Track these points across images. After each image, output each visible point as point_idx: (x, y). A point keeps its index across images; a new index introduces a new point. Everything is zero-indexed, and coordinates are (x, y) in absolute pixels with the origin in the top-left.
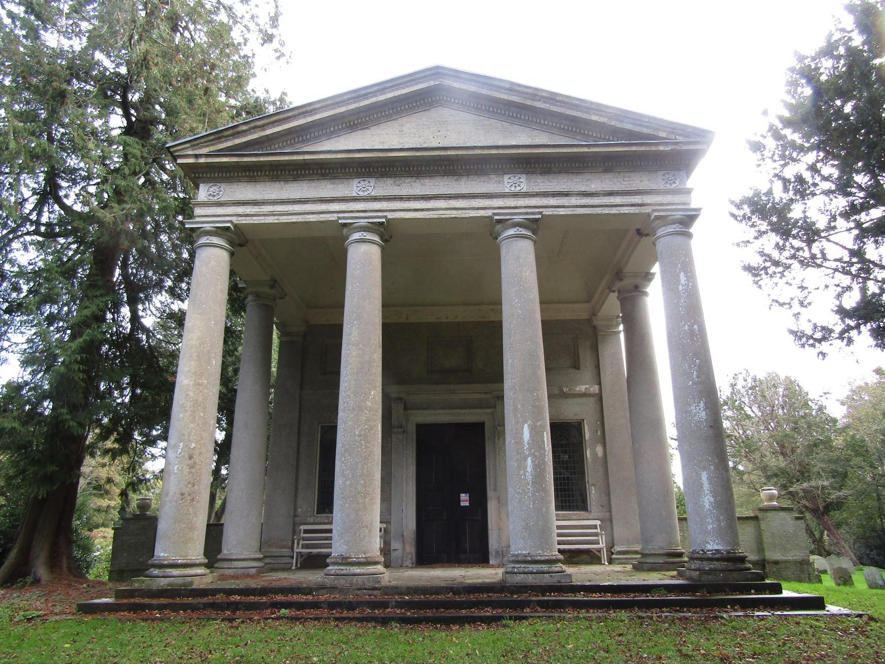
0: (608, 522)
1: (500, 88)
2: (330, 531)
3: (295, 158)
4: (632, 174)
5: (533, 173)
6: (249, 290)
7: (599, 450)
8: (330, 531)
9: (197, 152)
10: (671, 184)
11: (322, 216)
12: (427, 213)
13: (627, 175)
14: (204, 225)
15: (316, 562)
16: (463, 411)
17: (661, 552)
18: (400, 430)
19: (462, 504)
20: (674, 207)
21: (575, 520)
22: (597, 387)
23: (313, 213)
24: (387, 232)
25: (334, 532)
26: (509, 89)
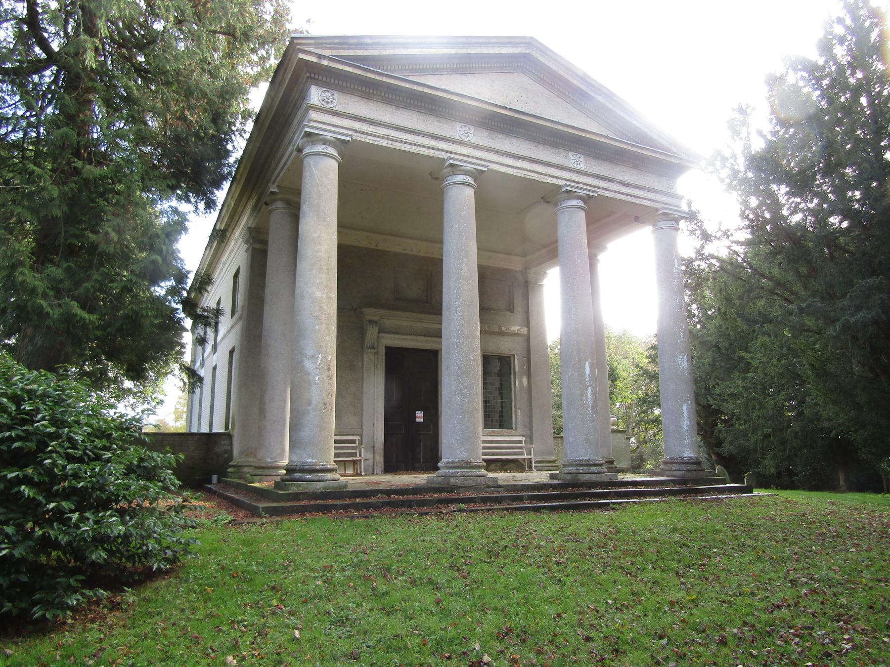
0: (530, 438)
1: (575, 75)
3: (535, 121)
6: (279, 196)
7: (525, 380)
9: (319, 52)
11: (432, 151)
12: (516, 171)
14: (325, 133)
18: (373, 351)
19: (418, 420)
21: (502, 437)
22: (526, 329)
23: (424, 147)
26: (581, 78)
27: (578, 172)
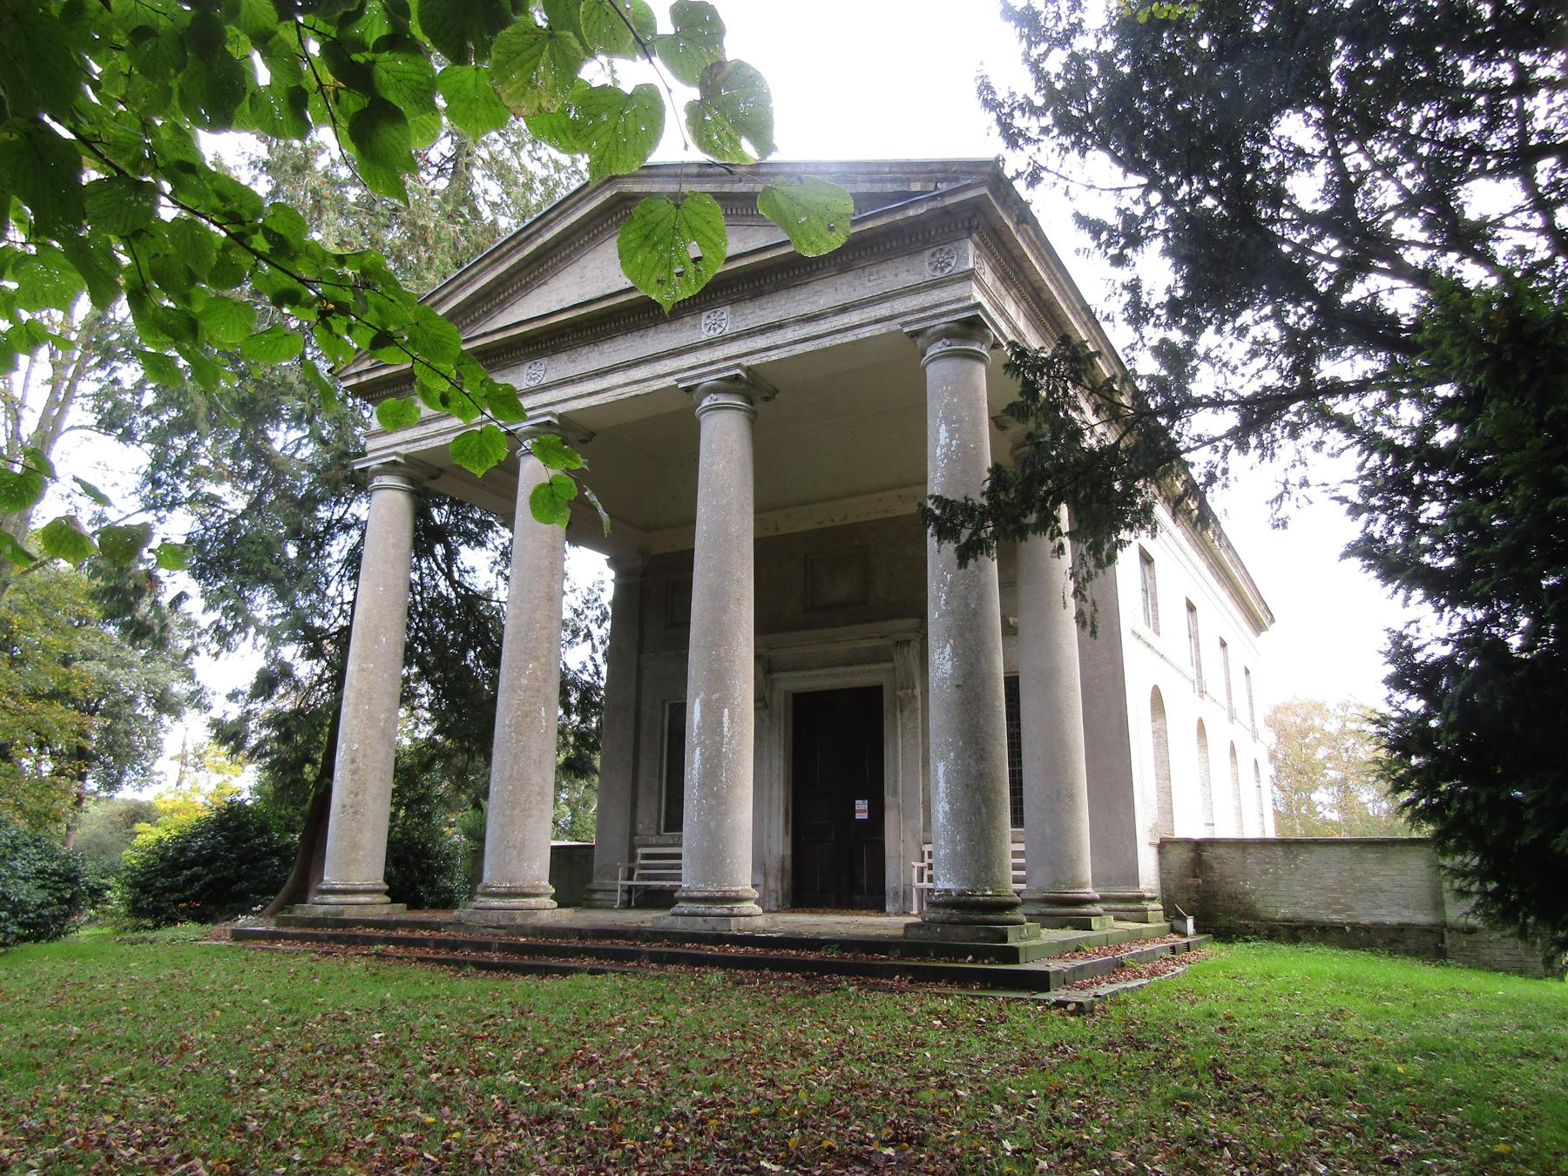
2: (679, 856)
4: (884, 266)
5: (739, 301)
8: (679, 856)
9: (359, 369)
10: (942, 269)
13: (874, 269)
15: (661, 899)
16: (850, 669)
17: (1037, 896)
19: (858, 816)
20: (944, 309)
24: (753, 389)
25: (684, 861)
27: (710, 344)
